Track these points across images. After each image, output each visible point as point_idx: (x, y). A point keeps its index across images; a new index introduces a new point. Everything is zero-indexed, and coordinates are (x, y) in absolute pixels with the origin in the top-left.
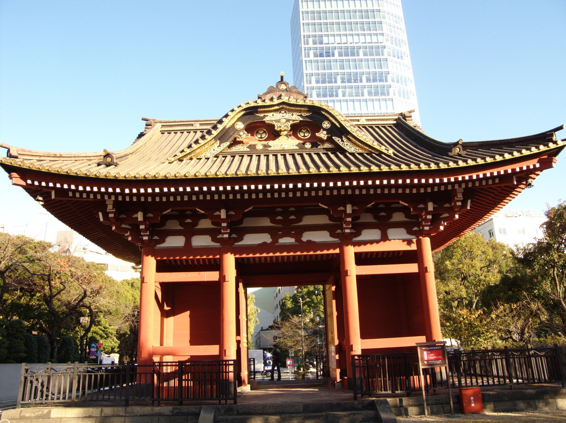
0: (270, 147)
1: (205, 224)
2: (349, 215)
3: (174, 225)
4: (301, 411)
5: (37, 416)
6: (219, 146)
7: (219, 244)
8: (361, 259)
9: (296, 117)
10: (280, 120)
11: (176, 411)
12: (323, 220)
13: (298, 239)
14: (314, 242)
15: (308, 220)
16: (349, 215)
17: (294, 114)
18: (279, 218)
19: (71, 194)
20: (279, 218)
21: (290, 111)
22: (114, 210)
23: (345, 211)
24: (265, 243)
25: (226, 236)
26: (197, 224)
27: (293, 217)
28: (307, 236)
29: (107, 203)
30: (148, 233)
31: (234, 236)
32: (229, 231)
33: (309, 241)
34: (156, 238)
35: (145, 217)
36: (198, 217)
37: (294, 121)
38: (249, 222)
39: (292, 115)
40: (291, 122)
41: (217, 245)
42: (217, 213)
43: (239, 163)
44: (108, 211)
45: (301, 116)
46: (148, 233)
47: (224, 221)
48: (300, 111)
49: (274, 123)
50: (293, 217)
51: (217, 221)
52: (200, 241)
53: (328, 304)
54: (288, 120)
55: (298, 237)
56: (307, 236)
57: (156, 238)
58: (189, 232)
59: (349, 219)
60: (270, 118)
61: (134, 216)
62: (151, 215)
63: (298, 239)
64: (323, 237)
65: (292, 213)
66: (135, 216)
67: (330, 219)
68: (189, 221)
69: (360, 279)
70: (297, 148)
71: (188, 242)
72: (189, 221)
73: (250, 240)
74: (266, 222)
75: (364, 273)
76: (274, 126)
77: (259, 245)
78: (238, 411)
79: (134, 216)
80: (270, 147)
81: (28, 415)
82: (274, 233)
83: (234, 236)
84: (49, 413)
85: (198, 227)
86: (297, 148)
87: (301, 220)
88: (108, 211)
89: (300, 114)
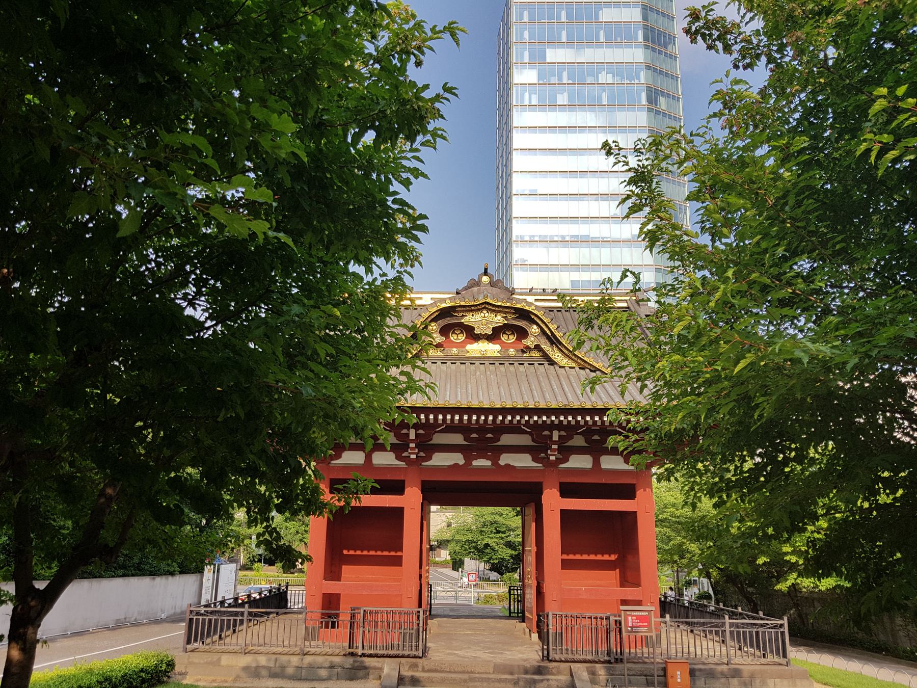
2: (555, 443)
4: (491, 671)
5: (207, 663)
8: (567, 491)
9: (499, 320)
11: (356, 665)
12: (525, 440)
13: (495, 462)
15: (507, 439)
16: (555, 443)
18: (475, 435)
20: (475, 435)
21: (492, 311)
23: (551, 436)
24: (456, 465)
27: (490, 435)
28: (506, 459)
31: (422, 454)
33: (507, 465)
38: (439, 439)
41: (402, 464)
43: (476, 614)
48: (505, 313)
50: (490, 435)
53: (526, 527)
59: (555, 447)
60: (470, 319)
63: (495, 462)
64: (523, 461)
67: (533, 440)
68: (596, 437)
69: (565, 514)
71: (596, 462)
72: (596, 437)
73: (440, 460)
74: (457, 439)
77: (449, 466)
78: (423, 668)
81: (196, 661)
83: (422, 454)
84: (219, 660)
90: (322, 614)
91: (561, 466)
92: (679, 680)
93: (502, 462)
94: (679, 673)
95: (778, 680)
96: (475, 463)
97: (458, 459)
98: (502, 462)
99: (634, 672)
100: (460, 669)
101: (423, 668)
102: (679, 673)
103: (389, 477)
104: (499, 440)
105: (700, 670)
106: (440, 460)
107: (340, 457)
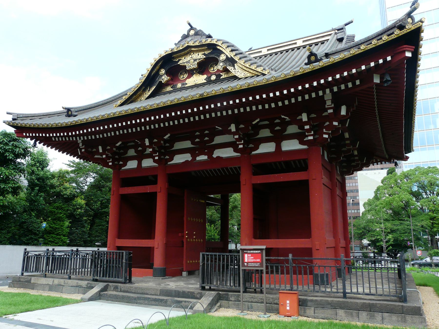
0: (187, 84)
1: (292, 129)
3: (265, 133)
6: (149, 90)
7: (239, 154)
10: (189, 61)
11: (89, 285)
14: (222, 158)
15: (218, 140)
17: (200, 54)
18: (197, 140)
19: (53, 139)
20: (197, 140)
22: (333, 106)
24: (187, 161)
25: (311, 138)
26: (285, 131)
27: (207, 138)
28: (217, 153)
29: (325, 99)
30: (242, 142)
32: (312, 133)
33: (218, 157)
34: (251, 146)
35: (237, 128)
36: (285, 124)
37: (199, 59)
39: (198, 55)
40: (198, 61)
41: (305, 147)
42: (299, 118)
44: (326, 107)
45: (204, 54)
46: (242, 142)
47: (306, 123)
49: (186, 64)
50: (207, 138)
51: (301, 125)
52: (291, 145)
54: (195, 60)
55: (210, 154)
56: (217, 153)
57: (251, 146)
58: (278, 138)
61: (298, 118)
62: (242, 126)
65: (207, 135)
66: (299, 118)
68: (278, 128)
70: (206, 81)
71: (278, 147)
72: (278, 128)
73: (179, 159)
74: (187, 144)
75: (268, 182)
76: (185, 66)
79: (298, 118)
80: (187, 84)
82: (193, 152)
85: (286, 133)
86: (206, 81)
87: (213, 141)
88: (326, 107)
89: (204, 53)
90: (281, 274)
91: (253, 153)
92: (288, 308)
93: (215, 156)
94: (288, 302)
95: (386, 315)
96: (198, 158)
97: (187, 157)
98: (215, 156)
99: (256, 300)
100: (141, 292)
101: (121, 290)
102: (288, 302)
103: (263, 161)
104: (213, 141)
105: (312, 301)
106: (179, 159)
107: (126, 165)
